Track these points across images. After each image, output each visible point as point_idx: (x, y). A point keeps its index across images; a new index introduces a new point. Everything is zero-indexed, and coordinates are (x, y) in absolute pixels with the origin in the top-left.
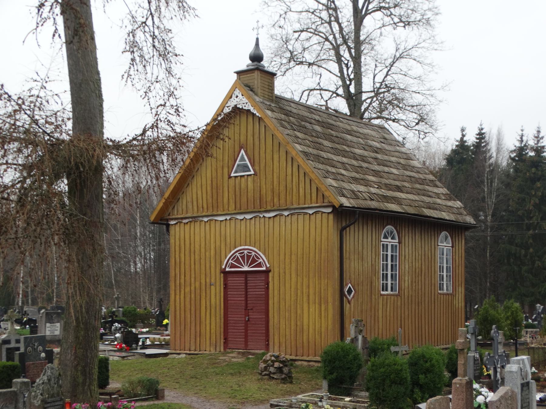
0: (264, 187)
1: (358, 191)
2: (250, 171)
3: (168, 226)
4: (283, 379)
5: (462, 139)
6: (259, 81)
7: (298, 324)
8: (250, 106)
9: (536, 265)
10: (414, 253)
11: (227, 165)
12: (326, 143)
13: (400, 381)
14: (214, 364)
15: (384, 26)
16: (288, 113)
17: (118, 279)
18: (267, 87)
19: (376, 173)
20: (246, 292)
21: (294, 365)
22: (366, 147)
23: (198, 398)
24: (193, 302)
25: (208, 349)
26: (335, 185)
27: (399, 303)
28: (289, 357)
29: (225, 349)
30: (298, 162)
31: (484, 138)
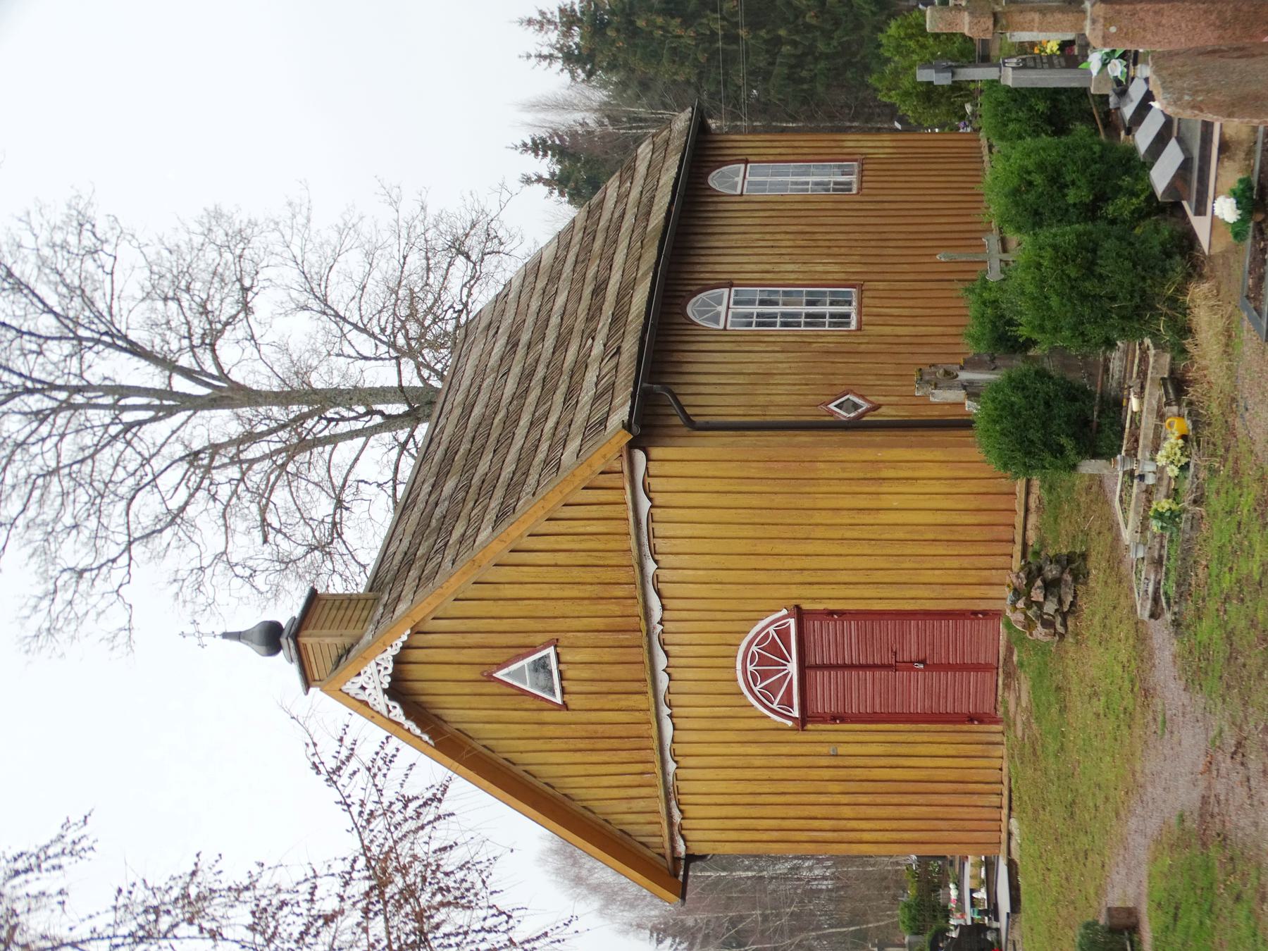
0: (585, 621)
1: (596, 385)
2: (547, 657)
3: (691, 858)
4: (1075, 579)
5: (546, 183)
6: (325, 631)
7: (931, 536)
8: (384, 656)
9: (814, 22)
10: (756, 250)
11: (535, 714)
12: (483, 467)
13: (1088, 251)
14: (1034, 753)
15: (252, 337)
16: (408, 561)
17: (846, 917)
18: (342, 612)
19: (561, 343)
20: (852, 667)
21: (1037, 547)
22: (503, 370)
23: (1131, 812)
24: (879, 799)
25: (997, 763)
26: (578, 442)
27: (881, 285)
28: (1017, 563)
29: (997, 722)
30: (521, 536)
31: (544, 141)
